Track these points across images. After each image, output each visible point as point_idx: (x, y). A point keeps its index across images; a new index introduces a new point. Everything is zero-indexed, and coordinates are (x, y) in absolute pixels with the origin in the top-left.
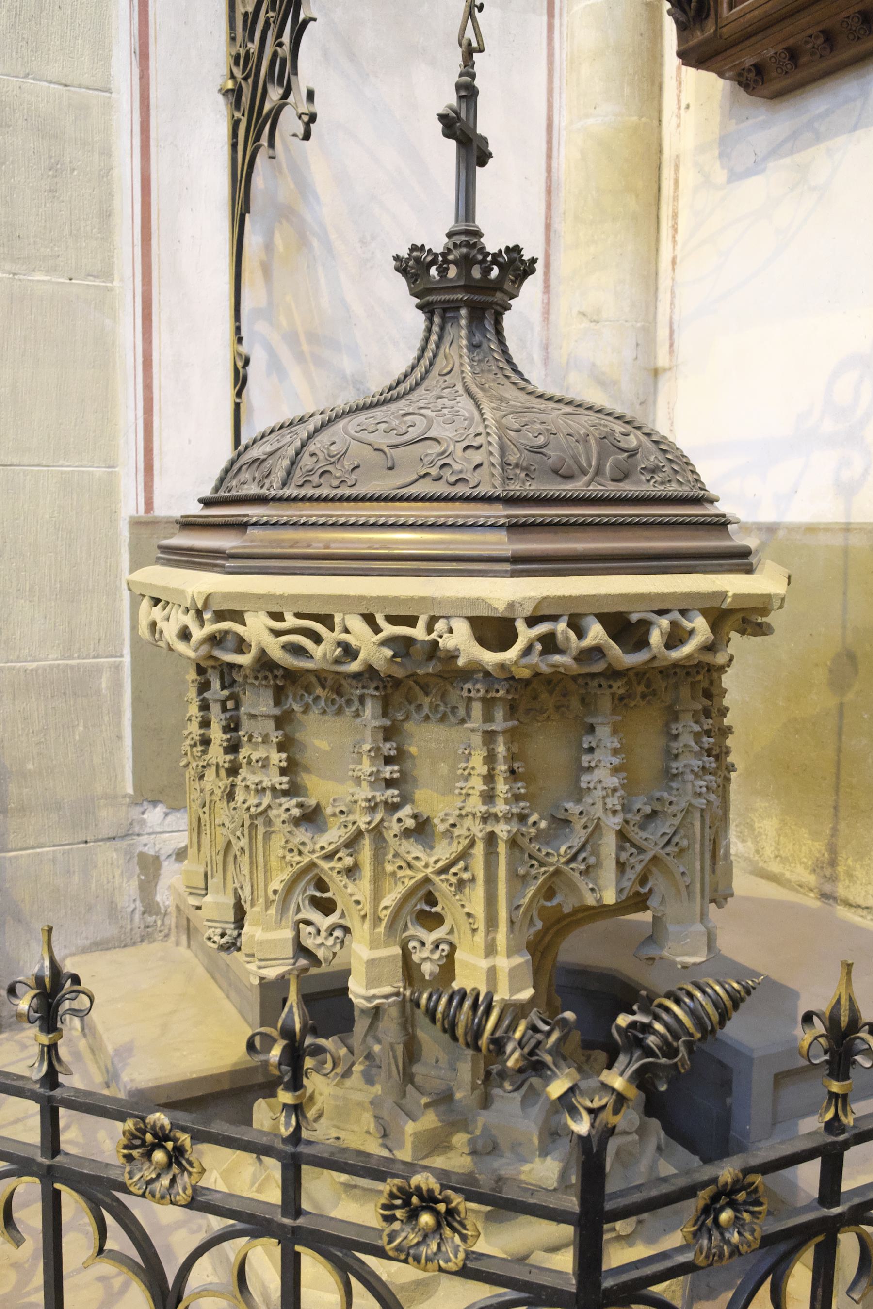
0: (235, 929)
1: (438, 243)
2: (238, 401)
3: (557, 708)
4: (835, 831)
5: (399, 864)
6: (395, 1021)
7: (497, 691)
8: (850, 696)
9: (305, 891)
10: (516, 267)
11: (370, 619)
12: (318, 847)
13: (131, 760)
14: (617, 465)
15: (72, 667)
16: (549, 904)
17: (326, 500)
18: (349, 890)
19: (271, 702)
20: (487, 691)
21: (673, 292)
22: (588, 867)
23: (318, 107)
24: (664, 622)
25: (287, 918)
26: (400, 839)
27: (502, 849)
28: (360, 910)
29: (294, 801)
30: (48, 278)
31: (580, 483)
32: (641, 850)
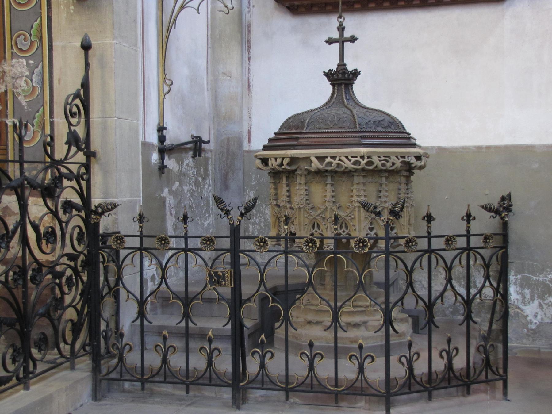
1: (335, 68)
10: (356, 74)
11: (347, 157)
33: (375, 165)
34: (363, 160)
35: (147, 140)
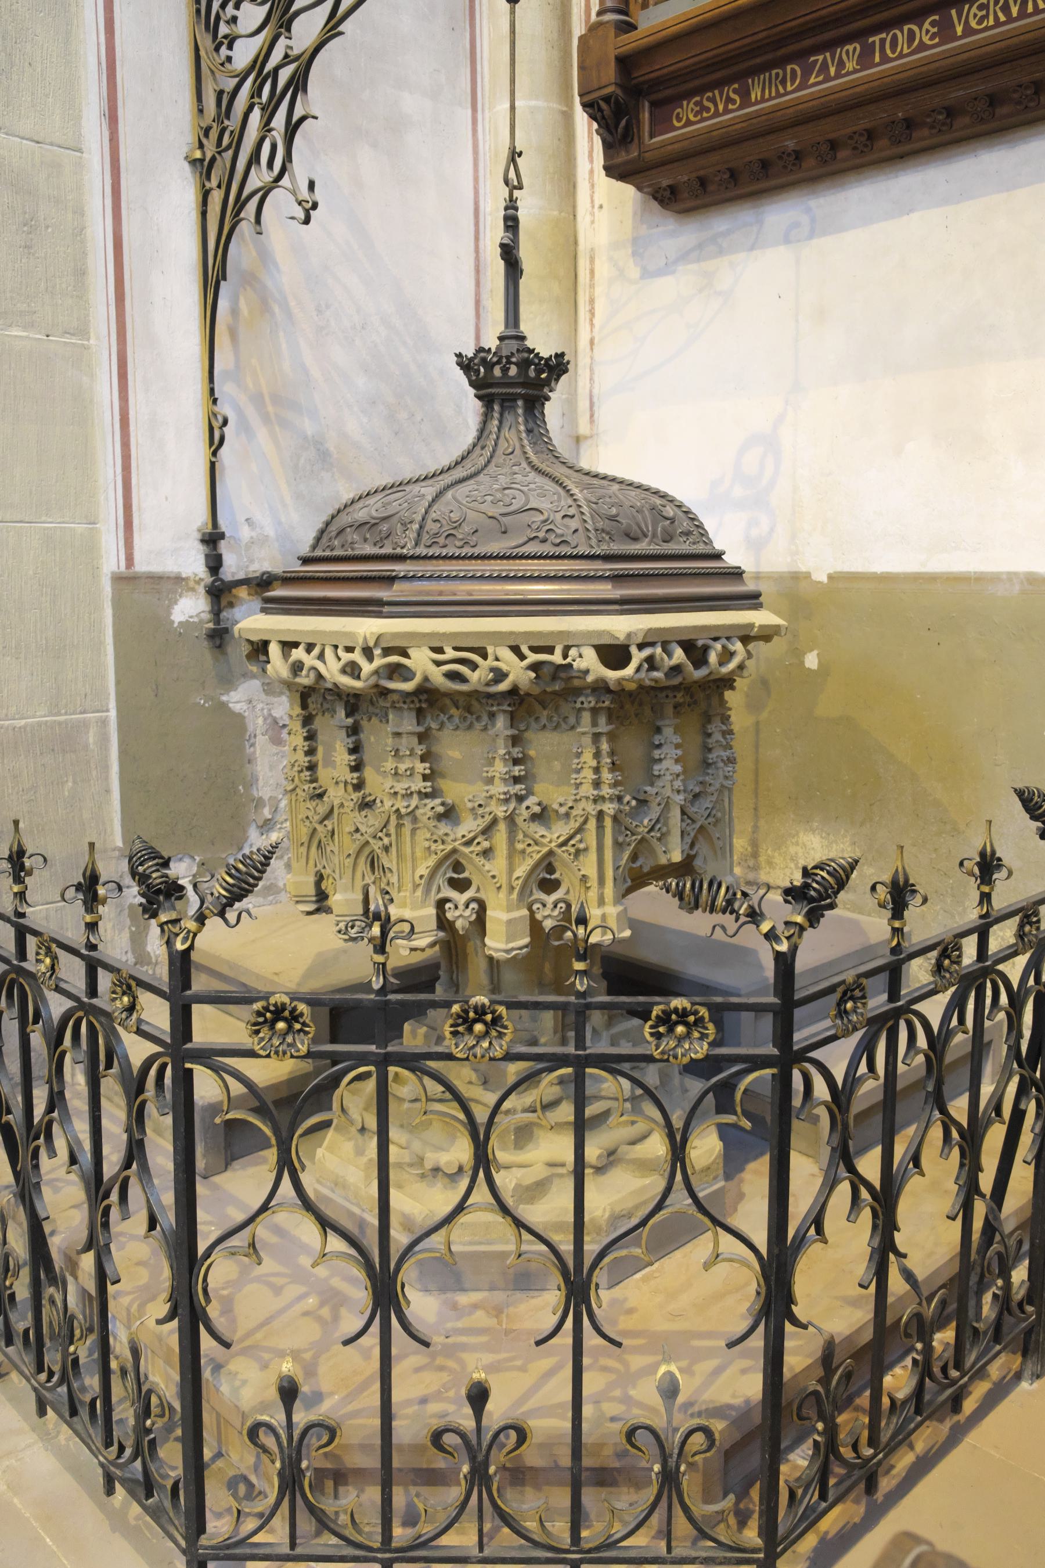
2: (213, 459)
3: (637, 715)
4: (756, 828)
8: (765, 715)
10: (557, 367)
11: (516, 650)
12: (459, 835)
13: (119, 813)
14: (664, 530)
15: (60, 723)
16: (634, 866)
17: (452, 558)
19: (415, 721)
21: (591, 370)
22: (662, 835)
23: (319, 195)
24: (718, 646)
27: (608, 822)
30: (25, 334)
31: (644, 544)
32: (693, 821)
34: (370, 658)
35: (142, 565)
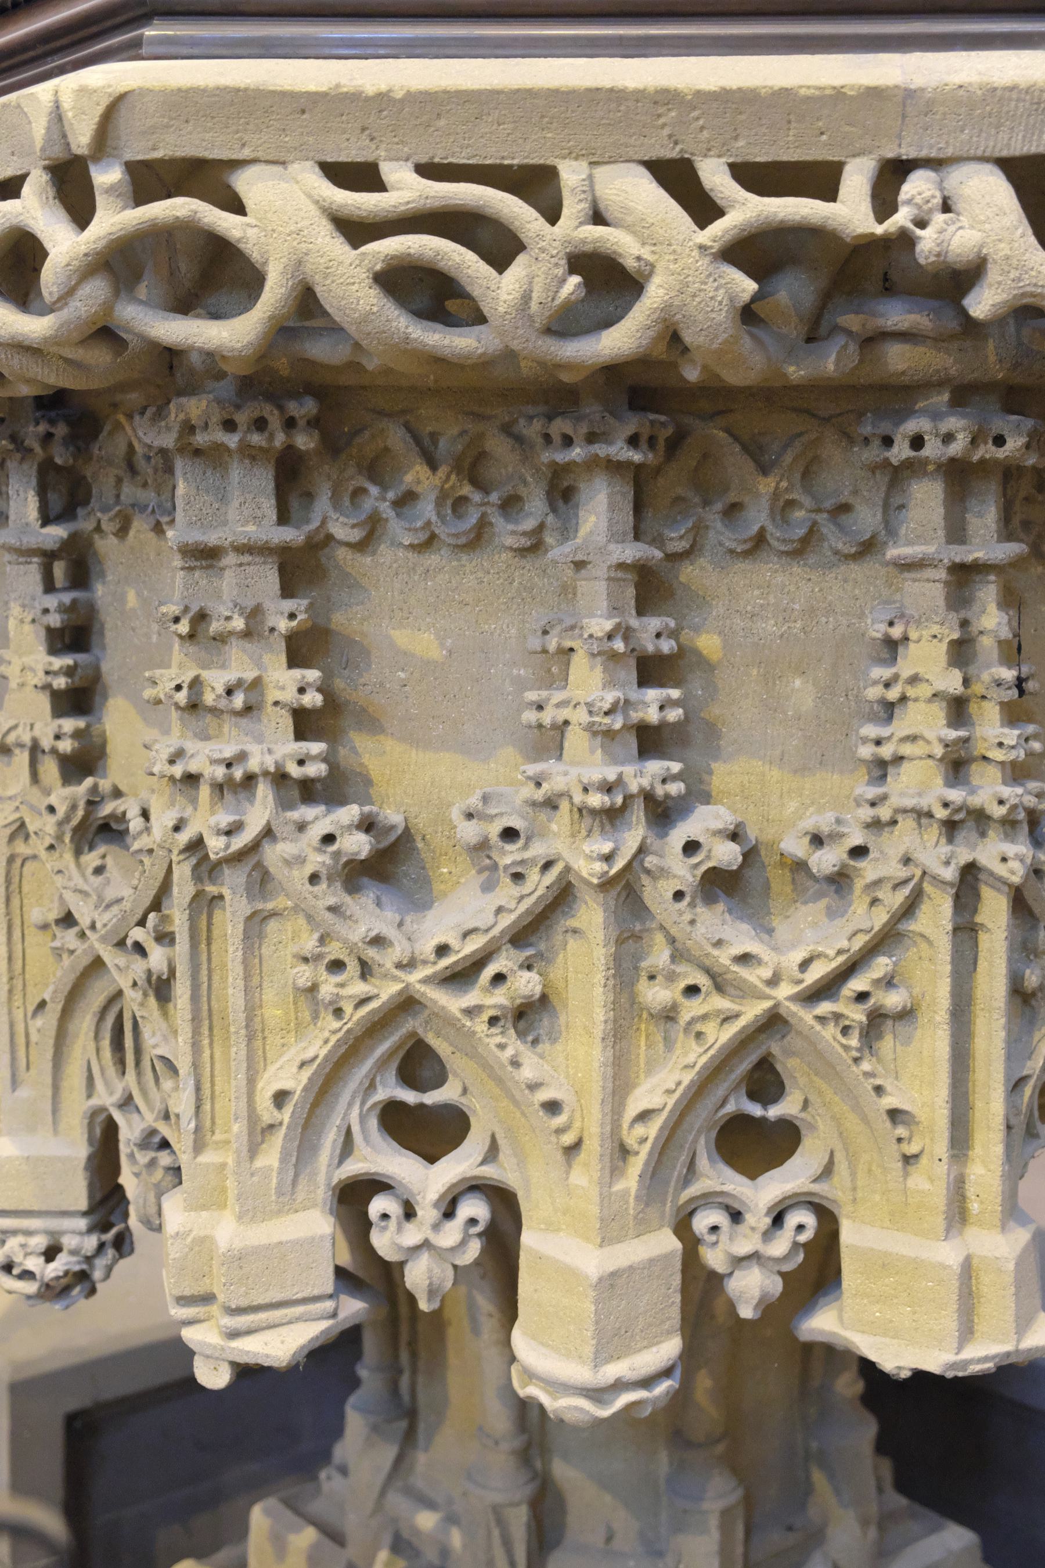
0: (90, 1230)
5: (690, 981)
6: (505, 1446)
7: (1000, 441)
9: (372, 1087)
11: (678, 178)
12: (427, 948)
18: (527, 1073)
19: (269, 508)
20: (974, 442)
25: (315, 1173)
26: (692, 905)
27: (994, 911)
28: (560, 1131)
29: (350, 813)
33: (274, 293)
